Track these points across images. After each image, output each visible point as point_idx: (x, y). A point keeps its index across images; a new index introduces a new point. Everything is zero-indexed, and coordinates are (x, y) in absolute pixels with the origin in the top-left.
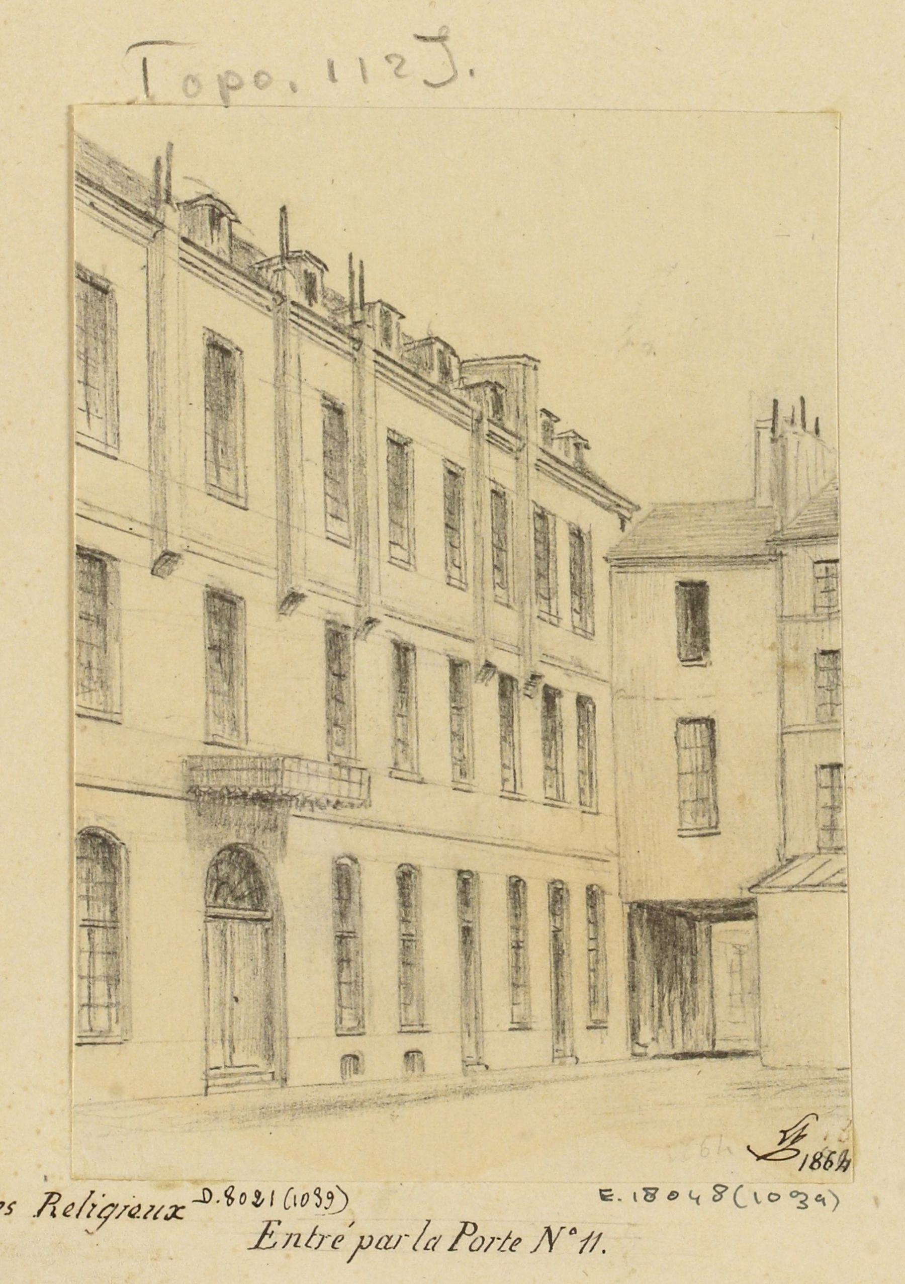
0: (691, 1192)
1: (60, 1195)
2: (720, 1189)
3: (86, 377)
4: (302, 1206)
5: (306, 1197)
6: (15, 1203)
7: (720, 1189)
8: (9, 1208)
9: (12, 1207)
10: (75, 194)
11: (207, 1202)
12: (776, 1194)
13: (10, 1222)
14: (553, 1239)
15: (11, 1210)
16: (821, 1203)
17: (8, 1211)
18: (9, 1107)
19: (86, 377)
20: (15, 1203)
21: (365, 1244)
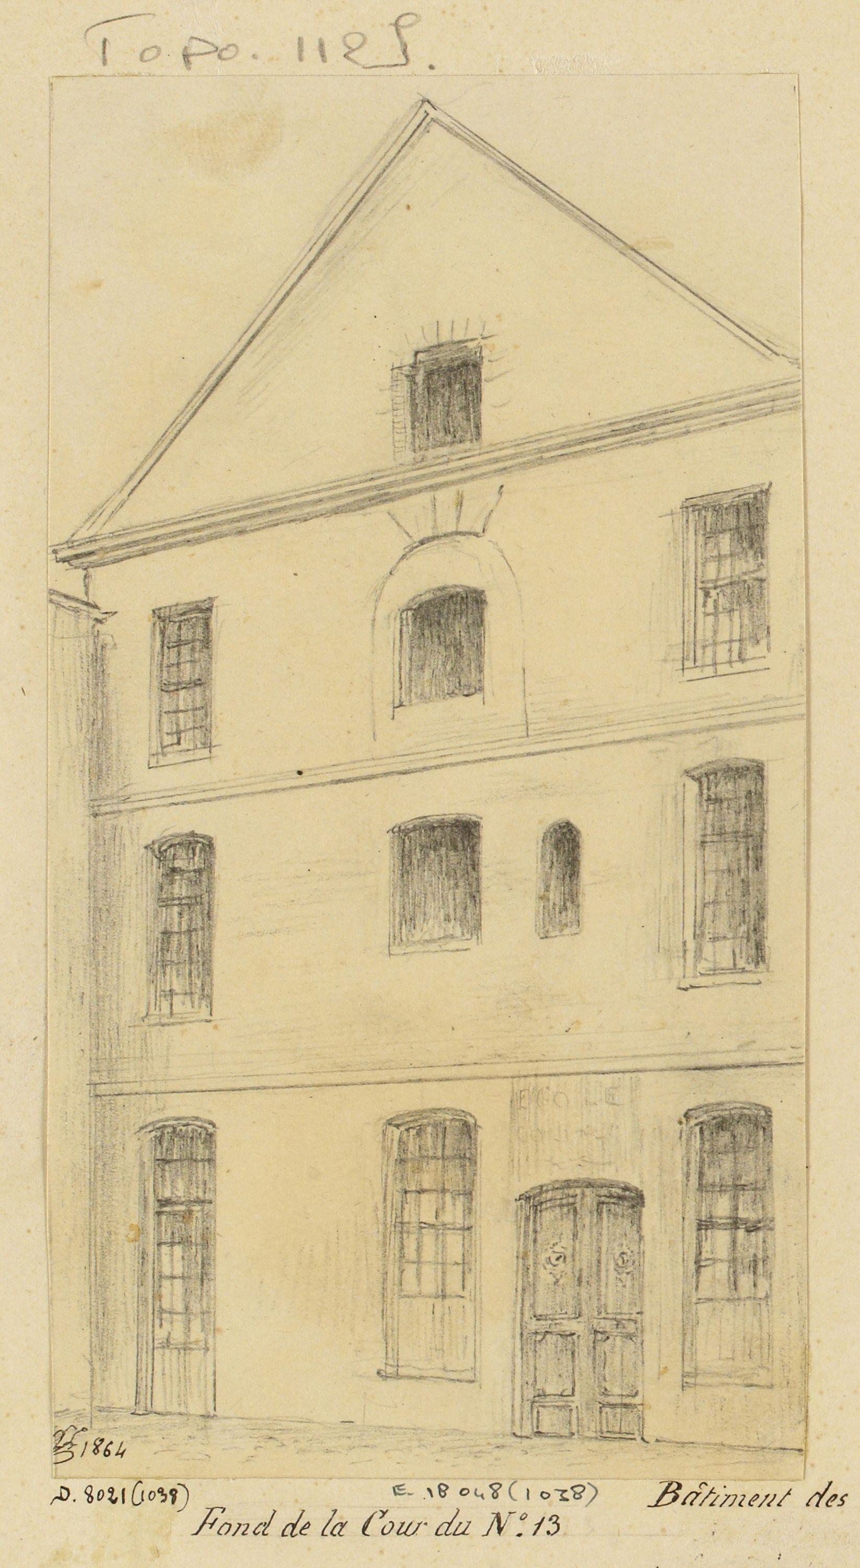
0: (476, 1490)
1: (102, 1490)
2: (496, 1487)
3: (191, 729)
4: (99, 1500)
5: (101, 1493)
6: (846, 1495)
7: (496, 1487)
8: (842, 1499)
9: (844, 1499)
10: (441, 495)
11: (65, 1500)
12: (547, 1493)
13: (842, 1512)
14: (502, 1526)
15: (843, 1502)
16: (480, 1498)
17: (841, 1503)
18: (841, 1408)
19: (191, 729)
20: (846, 1495)
21: (338, 1528)
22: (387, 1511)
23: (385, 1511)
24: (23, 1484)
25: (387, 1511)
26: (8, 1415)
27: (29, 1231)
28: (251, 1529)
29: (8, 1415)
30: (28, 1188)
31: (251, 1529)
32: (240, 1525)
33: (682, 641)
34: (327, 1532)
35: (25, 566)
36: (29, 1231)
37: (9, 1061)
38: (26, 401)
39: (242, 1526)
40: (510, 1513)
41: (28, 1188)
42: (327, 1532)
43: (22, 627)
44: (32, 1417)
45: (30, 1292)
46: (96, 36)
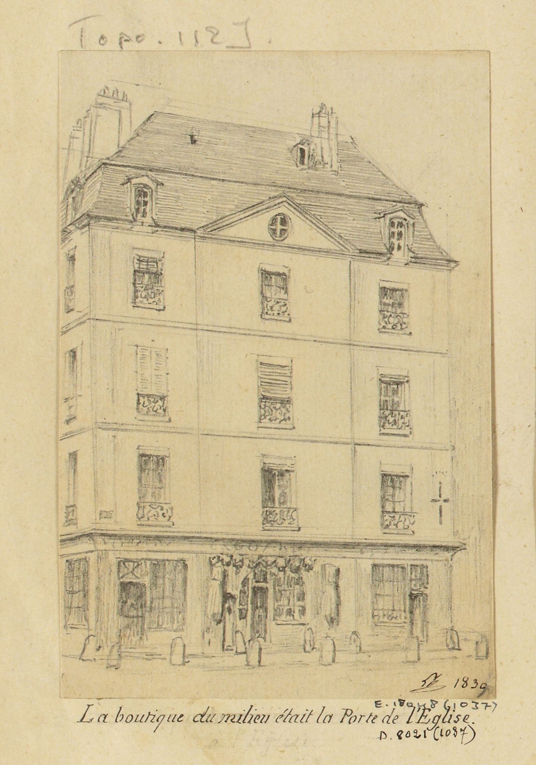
22: (485, 709)
23: (487, 708)
24: (522, 704)
25: (485, 709)
26: (512, 661)
27: (525, 546)
28: (166, 718)
29: (512, 661)
30: (525, 519)
31: (166, 718)
32: (449, 722)
33: (348, 346)
34: (321, 720)
35: (523, 132)
36: (525, 546)
37: (513, 440)
38: (523, 29)
39: (448, 720)
40: (89, 706)
41: (525, 519)
42: (321, 720)
43: (521, 170)
44: (528, 662)
45: (526, 584)
46: (77, 28)
